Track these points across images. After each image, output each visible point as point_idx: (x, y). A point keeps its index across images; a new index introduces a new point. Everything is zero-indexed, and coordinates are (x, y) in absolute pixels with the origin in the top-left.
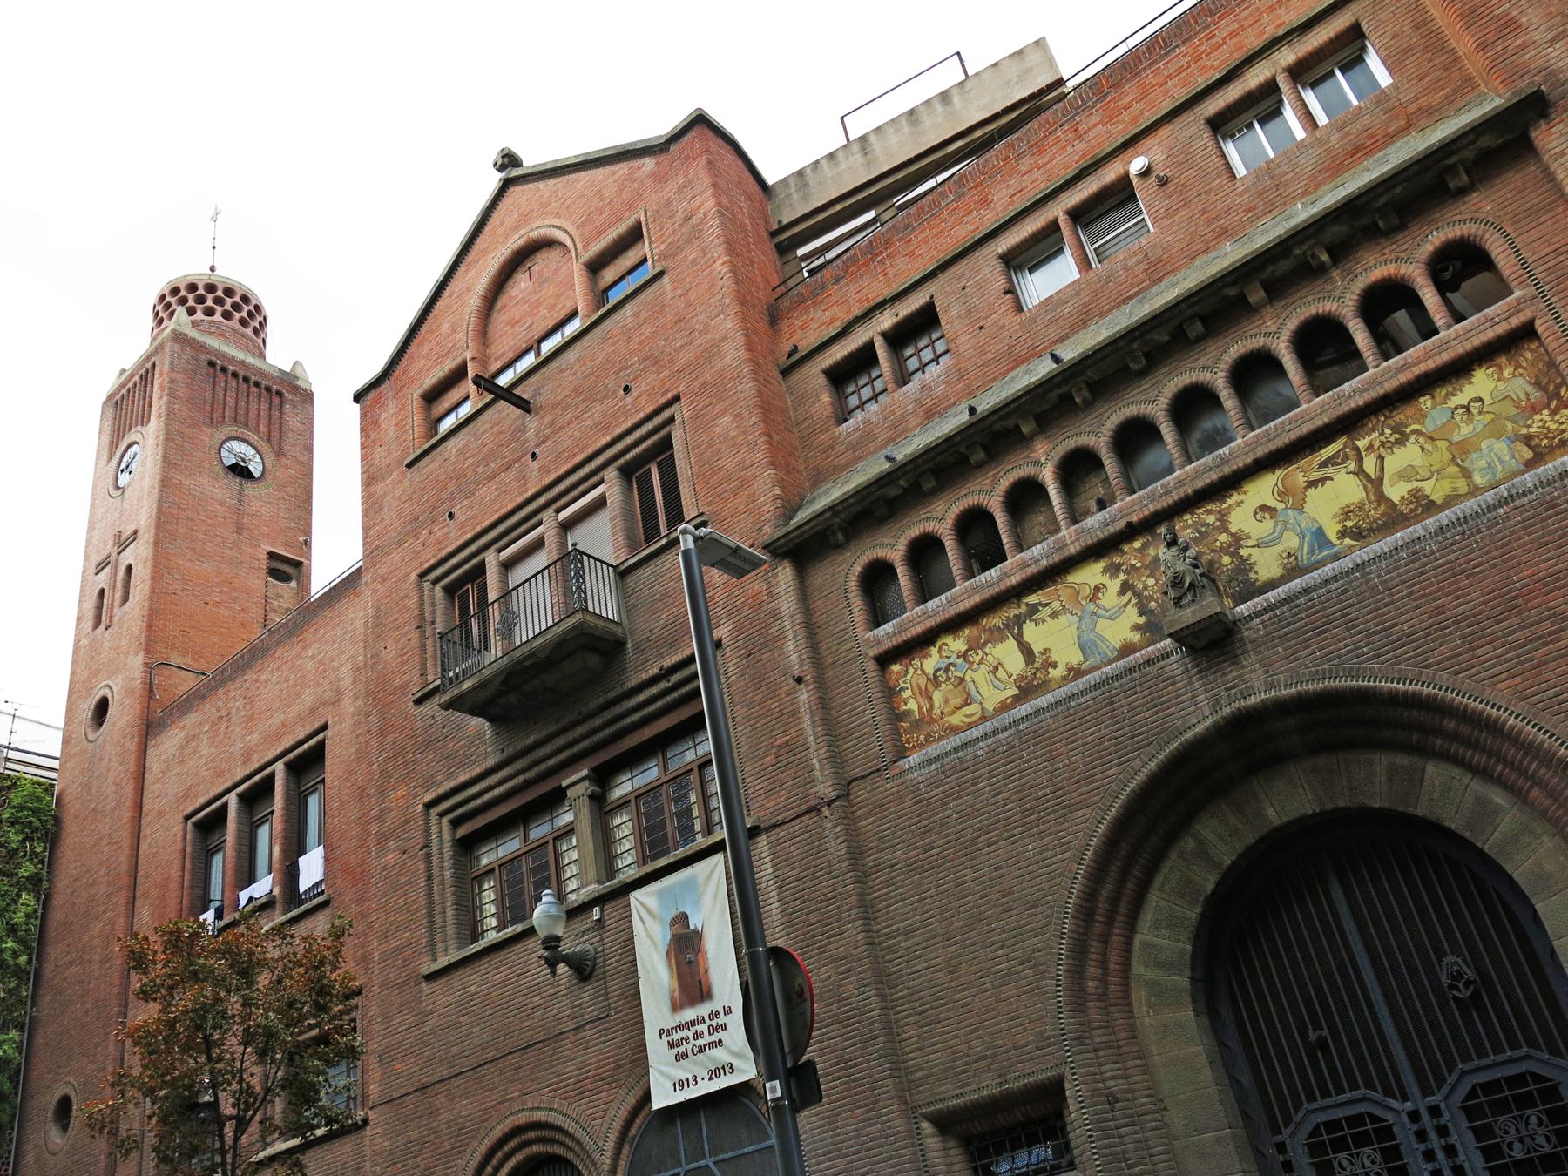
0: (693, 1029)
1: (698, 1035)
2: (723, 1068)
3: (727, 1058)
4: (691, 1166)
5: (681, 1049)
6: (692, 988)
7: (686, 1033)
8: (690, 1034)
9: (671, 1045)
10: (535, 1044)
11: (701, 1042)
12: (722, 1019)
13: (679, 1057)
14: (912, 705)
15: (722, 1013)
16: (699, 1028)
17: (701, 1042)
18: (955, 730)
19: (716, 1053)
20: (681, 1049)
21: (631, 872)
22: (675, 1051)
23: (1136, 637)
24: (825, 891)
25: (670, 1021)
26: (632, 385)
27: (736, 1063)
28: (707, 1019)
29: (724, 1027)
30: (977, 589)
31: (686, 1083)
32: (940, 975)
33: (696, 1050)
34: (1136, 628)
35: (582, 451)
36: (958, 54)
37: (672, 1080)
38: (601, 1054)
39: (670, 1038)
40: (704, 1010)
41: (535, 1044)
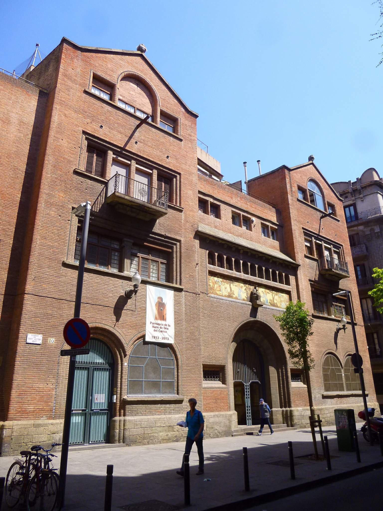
0: (160, 326)
1: (161, 328)
2: (166, 338)
3: (167, 336)
4: (151, 357)
5: (156, 329)
6: (161, 316)
7: (158, 326)
8: (159, 327)
9: (153, 327)
10: (108, 307)
11: (161, 330)
12: (167, 327)
13: (155, 331)
14: (211, 284)
15: (168, 325)
16: (162, 326)
17: (161, 330)
18: (217, 294)
19: (165, 334)
20: (156, 329)
21: (153, 279)
22: (154, 329)
23: (245, 299)
24: (195, 312)
25: (153, 321)
26: (169, 158)
27: (170, 338)
28: (164, 325)
29: (168, 329)
30: (227, 272)
31: (156, 337)
32: (210, 339)
33: (160, 331)
34: (245, 297)
35: (152, 158)
36: (64, 40)
37: (152, 335)
38: (131, 320)
39: (153, 325)
40: (163, 322)
41: (108, 307)
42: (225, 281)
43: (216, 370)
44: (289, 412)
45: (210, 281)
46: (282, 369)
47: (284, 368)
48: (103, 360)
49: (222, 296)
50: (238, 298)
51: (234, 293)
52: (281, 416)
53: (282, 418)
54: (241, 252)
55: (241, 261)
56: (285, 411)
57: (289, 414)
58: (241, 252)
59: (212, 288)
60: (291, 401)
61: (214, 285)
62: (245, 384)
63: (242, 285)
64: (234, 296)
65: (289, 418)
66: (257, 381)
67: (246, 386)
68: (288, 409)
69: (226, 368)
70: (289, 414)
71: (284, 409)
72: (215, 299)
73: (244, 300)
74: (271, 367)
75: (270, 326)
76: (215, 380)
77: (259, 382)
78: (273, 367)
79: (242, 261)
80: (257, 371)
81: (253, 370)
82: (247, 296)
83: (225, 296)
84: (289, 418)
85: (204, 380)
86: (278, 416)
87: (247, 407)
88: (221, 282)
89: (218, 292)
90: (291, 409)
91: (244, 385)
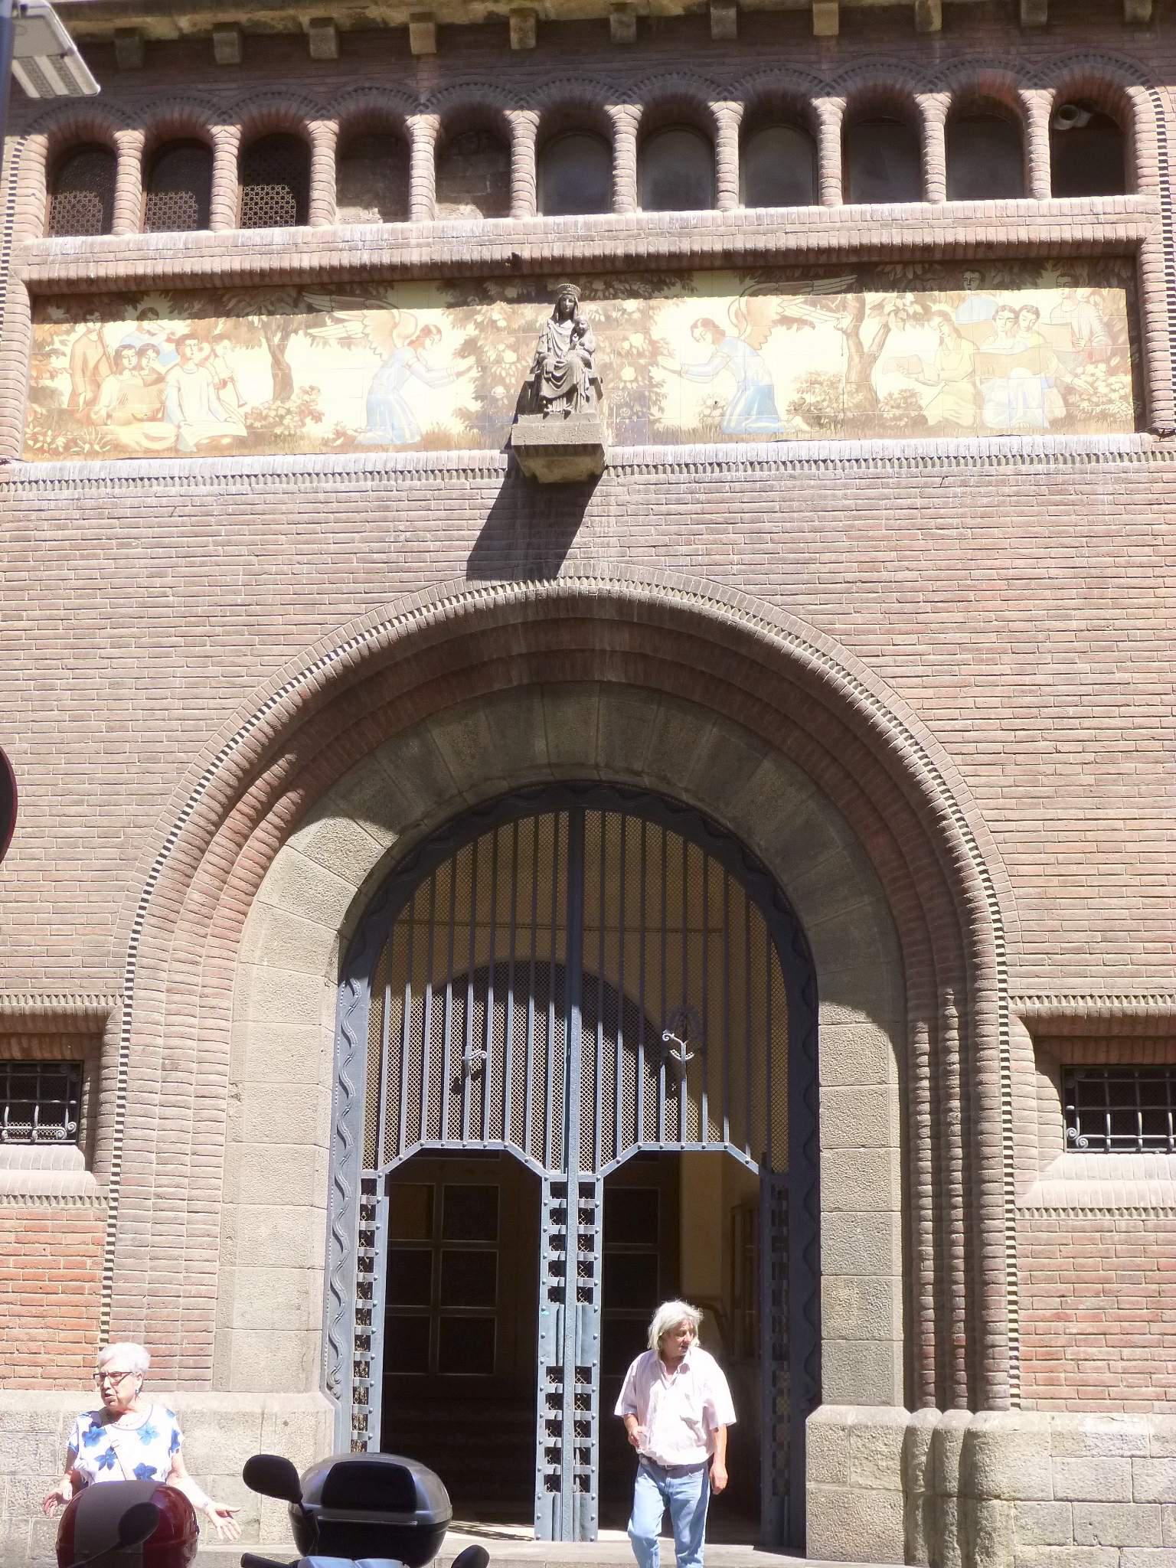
34: (463, 414)
42: (221, 324)
43: (38, 1054)
44: (955, 1447)
45: (56, 362)
46: (938, 1030)
47: (953, 1011)
48: (589, 1025)
49: (175, 452)
50: (361, 438)
51: (320, 406)
52: (896, 1482)
53: (899, 1499)
54: (421, 41)
55: (716, 106)
56: (928, 1438)
57: (953, 1466)
58: (421, 41)
59: (63, 417)
60: (999, 1339)
61: (98, 386)
62: (551, 1175)
63: (435, 316)
64: (314, 430)
65: (953, 1506)
66: (715, 1146)
67: (559, 1190)
68: (960, 1419)
69: (114, 1037)
70: (953, 1466)
71: (930, 1418)
72: (66, 493)
73: (435, 441)
74: (842, 1013)
75: (750, 625)
76: (28, 1139)
77: (745, 1157)
78: (861, 1017)
79: (333, 125)
80: (701, 1051)
81: (658, 1056)
82: (475, 406)
83: (214, 448)
84: (953, 1506)
85: (1071, 1143)
86: (854, 1478)
87: (557, 1373)
88: (180, 342)
89: (130, 436)
90: (987, 1422)
91: (537, 1180)
